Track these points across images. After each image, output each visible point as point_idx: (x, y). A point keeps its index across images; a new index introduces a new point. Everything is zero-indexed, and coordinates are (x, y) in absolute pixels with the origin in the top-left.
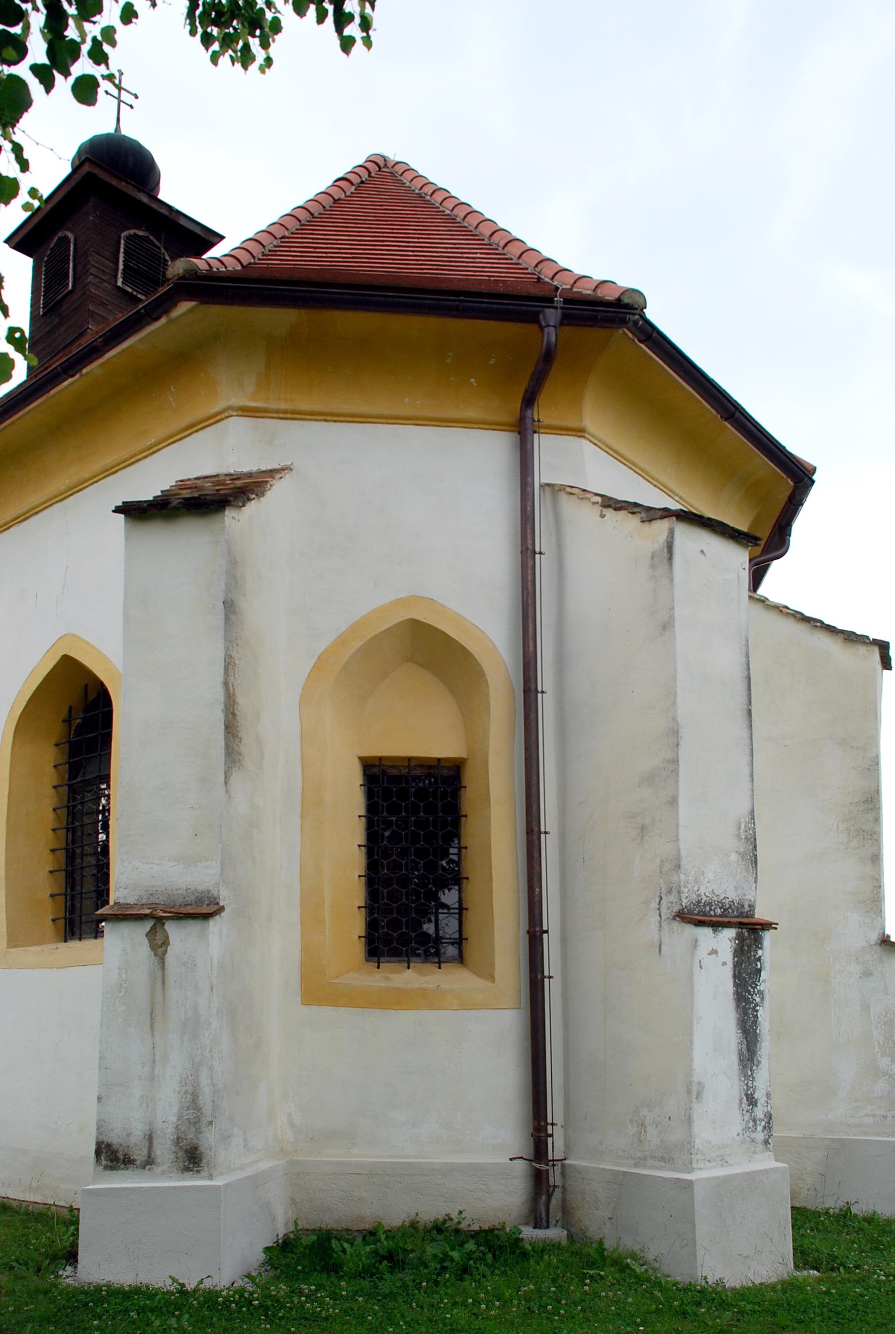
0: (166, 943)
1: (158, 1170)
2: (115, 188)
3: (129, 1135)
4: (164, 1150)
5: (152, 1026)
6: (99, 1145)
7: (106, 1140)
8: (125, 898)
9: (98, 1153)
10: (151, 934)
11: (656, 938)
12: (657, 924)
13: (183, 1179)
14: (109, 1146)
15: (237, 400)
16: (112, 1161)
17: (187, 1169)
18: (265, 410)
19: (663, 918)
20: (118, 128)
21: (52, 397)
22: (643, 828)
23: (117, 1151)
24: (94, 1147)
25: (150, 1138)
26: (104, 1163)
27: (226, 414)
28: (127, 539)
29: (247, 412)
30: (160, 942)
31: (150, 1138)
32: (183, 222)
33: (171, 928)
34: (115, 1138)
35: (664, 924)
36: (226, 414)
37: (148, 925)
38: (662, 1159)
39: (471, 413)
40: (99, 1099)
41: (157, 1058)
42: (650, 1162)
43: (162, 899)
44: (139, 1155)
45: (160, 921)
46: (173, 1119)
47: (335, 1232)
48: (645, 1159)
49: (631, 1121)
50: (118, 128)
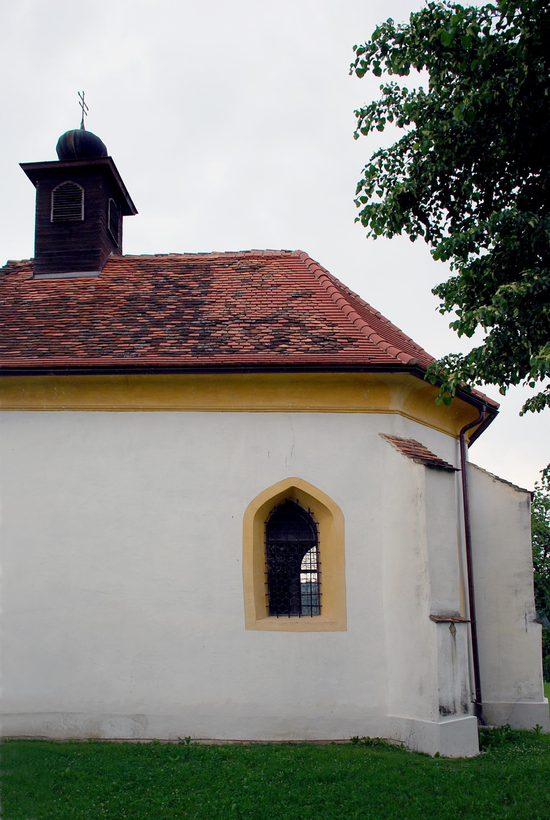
0: (455, 631)
1: (457, 714)
2: (113, 175)
3: (448, 702)
4: (459, 707)
5: (453, 662)
6: (440, 707)
7: (442, 705)
8: (434, 613)
9: (440, 710)
10: (450, 628)
11: (524, 627)
12: (525, 623)
13: (464, 717)
14: (443, 707)
15: (399, 408)
16: (444, 713)
17: (465, 713)
18: (407, 415)
19: (528, 621)
20: (83, 127)
21: (181, 321)
22: (516, 591)
23: (445, 709)
24: (439, 708)
25: (454, 703)
26: (442, 714)
27: (396, 412)
28: (426, 475)
29: (403, 414)
30: (453, 631)
31: (454, 703)
32: (128, 201)
33: (456, 625)
34: (444, 704)
35: (528, 623)
36: (396, 412)
37: (450, 624)
38: (530, 698)
39: (447, 429)
40: (439, 690)
41: (455, 673)
42: (523, 699)
43: (445, 614)
44: (452, 710)
45: (453, 623)
46: (460, 695)
47: (55, 742)
48: (522, 698)
49: (514, 686)
50: (83, 127)
